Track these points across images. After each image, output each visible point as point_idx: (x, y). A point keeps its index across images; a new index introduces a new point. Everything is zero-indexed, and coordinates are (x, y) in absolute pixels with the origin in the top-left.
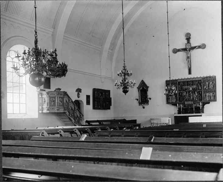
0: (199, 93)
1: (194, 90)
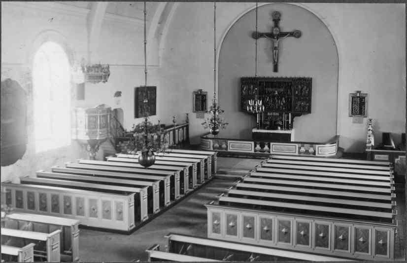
1: (281, 96)
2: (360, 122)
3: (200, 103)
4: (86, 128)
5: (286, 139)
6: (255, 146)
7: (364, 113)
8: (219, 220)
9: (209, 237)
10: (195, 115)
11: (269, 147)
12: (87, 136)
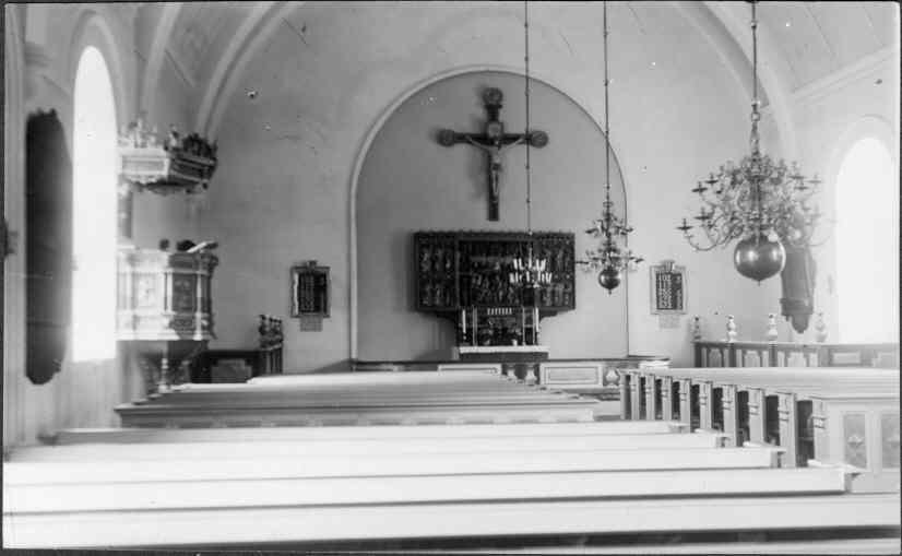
2: (673, 326)
3: (310, 296)
4: (166, 308)
7: (681, 305)
10: (296, 323)
11: (537, 373)
12: (173, 331)
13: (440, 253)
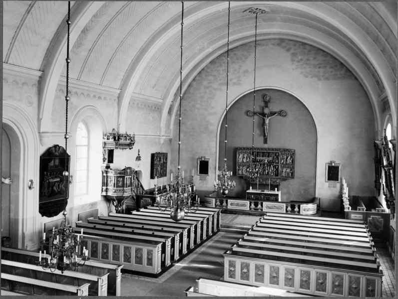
0: (274, 167)
1: (270, 163)
2: (334, 187)
5: (275, 198)
6: (250, 205)
8: (234, 267)
9: (225, 280)
11: (262, 206)
13: (245, 156)
